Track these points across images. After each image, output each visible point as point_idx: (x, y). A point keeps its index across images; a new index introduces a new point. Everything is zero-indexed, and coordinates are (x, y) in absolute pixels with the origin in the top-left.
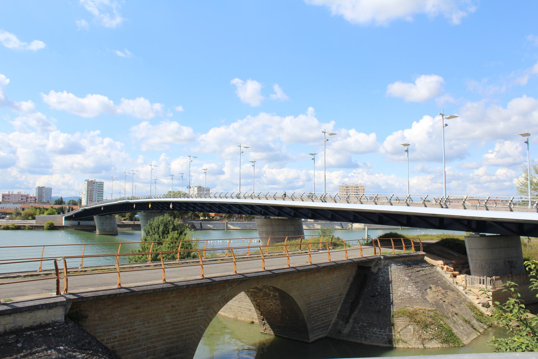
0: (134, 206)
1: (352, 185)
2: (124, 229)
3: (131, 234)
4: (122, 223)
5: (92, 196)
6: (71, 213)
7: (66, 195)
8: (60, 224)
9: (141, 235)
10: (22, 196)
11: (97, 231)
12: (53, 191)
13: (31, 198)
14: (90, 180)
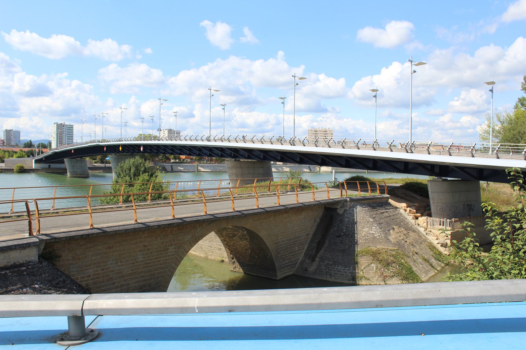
0: (105, 149)
1: (320, 129)
2: (95, 171)
5: (62, 139)
6: (41, 156)
7: (36, 138)
8: (30, 167)
11: (68, 174)
12: (21, 134)
14: (59, 123)
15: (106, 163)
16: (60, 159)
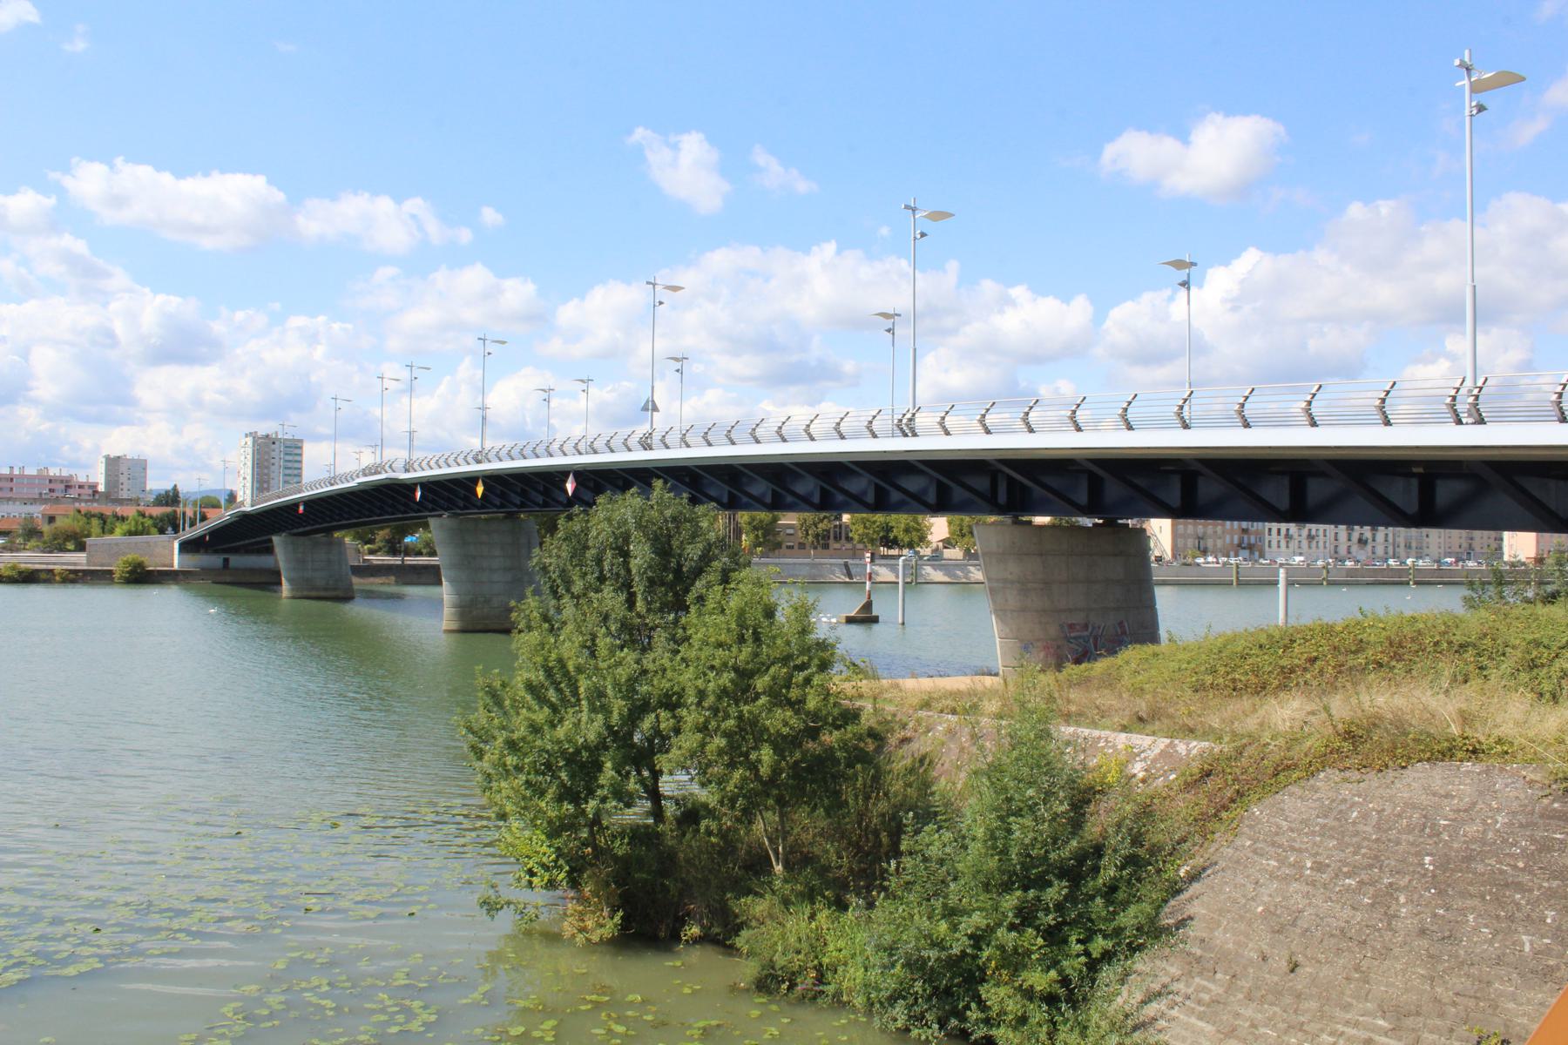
0: (419, 494)
2: (372, 580)
4: (365, 560)
5: (268, 482)
6: (200, 529)
7: (191, 484)
9: (443, 599)
10: (50, 481)
11: (286, 588)
12: (149, 472)
13: (80, 487)
14: (261, 433)
15: (407, 554)
16: (258, 539)
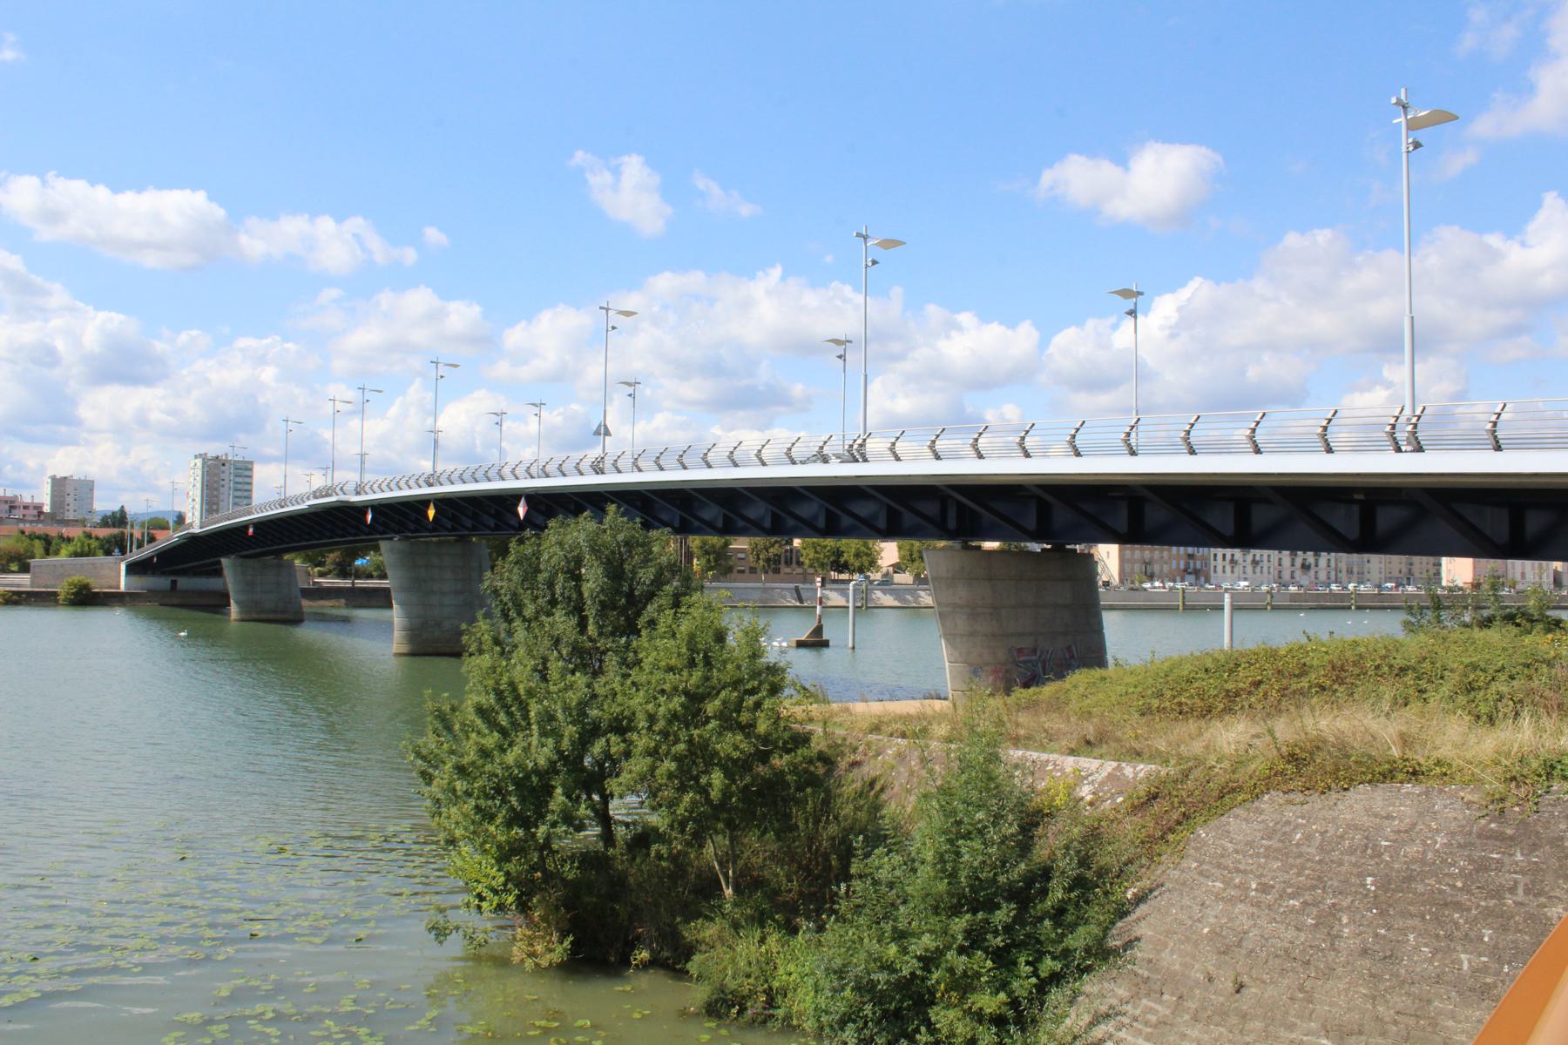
0: (370, 517)
2: (322, 602)
3: (346, 620)
4: (314, 583)
5: (217, 504)
6: (148, 551)
7: (138, 505)
8: (111, 588)
11: (234, 609)
12: (96, 493)
13: (26, 507)
14: (211, 454)
15: (358, 577)
